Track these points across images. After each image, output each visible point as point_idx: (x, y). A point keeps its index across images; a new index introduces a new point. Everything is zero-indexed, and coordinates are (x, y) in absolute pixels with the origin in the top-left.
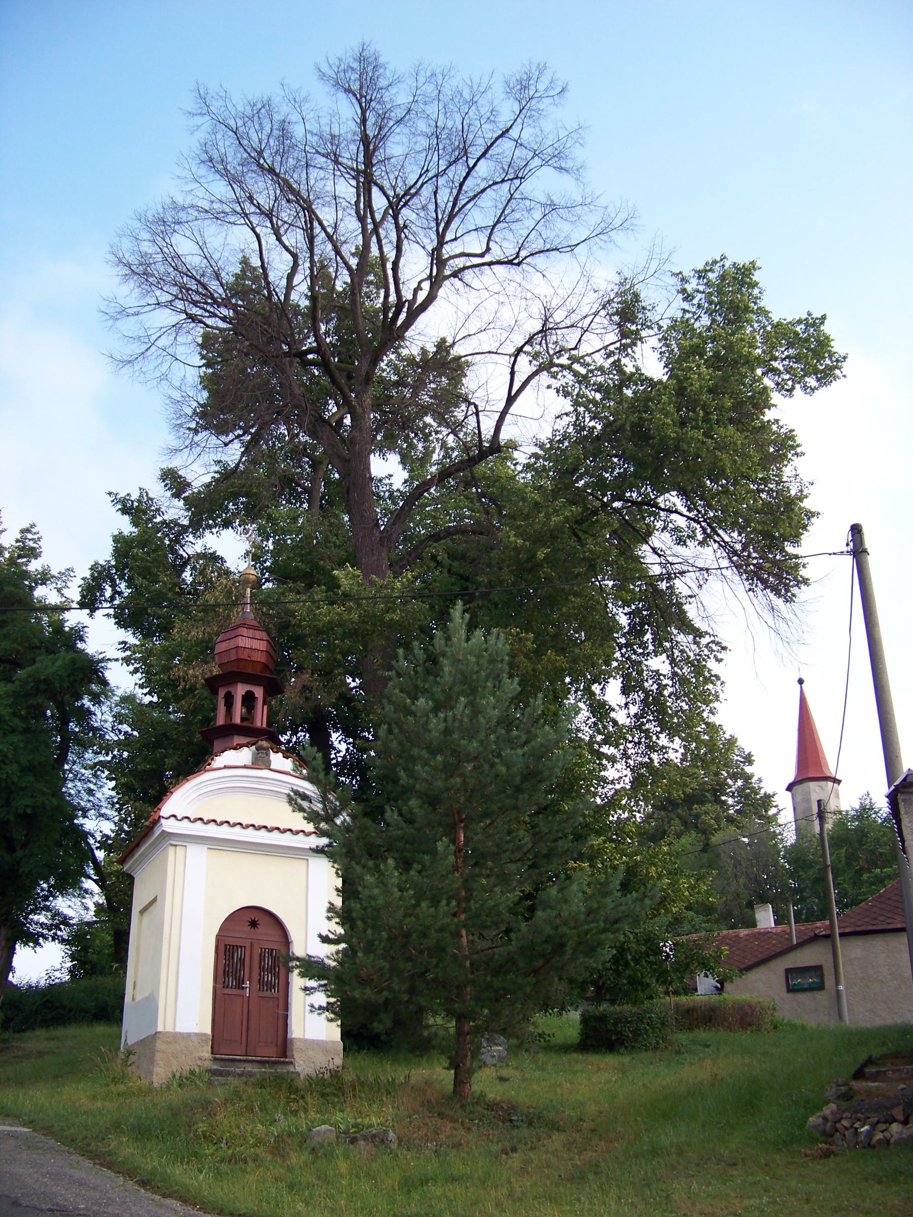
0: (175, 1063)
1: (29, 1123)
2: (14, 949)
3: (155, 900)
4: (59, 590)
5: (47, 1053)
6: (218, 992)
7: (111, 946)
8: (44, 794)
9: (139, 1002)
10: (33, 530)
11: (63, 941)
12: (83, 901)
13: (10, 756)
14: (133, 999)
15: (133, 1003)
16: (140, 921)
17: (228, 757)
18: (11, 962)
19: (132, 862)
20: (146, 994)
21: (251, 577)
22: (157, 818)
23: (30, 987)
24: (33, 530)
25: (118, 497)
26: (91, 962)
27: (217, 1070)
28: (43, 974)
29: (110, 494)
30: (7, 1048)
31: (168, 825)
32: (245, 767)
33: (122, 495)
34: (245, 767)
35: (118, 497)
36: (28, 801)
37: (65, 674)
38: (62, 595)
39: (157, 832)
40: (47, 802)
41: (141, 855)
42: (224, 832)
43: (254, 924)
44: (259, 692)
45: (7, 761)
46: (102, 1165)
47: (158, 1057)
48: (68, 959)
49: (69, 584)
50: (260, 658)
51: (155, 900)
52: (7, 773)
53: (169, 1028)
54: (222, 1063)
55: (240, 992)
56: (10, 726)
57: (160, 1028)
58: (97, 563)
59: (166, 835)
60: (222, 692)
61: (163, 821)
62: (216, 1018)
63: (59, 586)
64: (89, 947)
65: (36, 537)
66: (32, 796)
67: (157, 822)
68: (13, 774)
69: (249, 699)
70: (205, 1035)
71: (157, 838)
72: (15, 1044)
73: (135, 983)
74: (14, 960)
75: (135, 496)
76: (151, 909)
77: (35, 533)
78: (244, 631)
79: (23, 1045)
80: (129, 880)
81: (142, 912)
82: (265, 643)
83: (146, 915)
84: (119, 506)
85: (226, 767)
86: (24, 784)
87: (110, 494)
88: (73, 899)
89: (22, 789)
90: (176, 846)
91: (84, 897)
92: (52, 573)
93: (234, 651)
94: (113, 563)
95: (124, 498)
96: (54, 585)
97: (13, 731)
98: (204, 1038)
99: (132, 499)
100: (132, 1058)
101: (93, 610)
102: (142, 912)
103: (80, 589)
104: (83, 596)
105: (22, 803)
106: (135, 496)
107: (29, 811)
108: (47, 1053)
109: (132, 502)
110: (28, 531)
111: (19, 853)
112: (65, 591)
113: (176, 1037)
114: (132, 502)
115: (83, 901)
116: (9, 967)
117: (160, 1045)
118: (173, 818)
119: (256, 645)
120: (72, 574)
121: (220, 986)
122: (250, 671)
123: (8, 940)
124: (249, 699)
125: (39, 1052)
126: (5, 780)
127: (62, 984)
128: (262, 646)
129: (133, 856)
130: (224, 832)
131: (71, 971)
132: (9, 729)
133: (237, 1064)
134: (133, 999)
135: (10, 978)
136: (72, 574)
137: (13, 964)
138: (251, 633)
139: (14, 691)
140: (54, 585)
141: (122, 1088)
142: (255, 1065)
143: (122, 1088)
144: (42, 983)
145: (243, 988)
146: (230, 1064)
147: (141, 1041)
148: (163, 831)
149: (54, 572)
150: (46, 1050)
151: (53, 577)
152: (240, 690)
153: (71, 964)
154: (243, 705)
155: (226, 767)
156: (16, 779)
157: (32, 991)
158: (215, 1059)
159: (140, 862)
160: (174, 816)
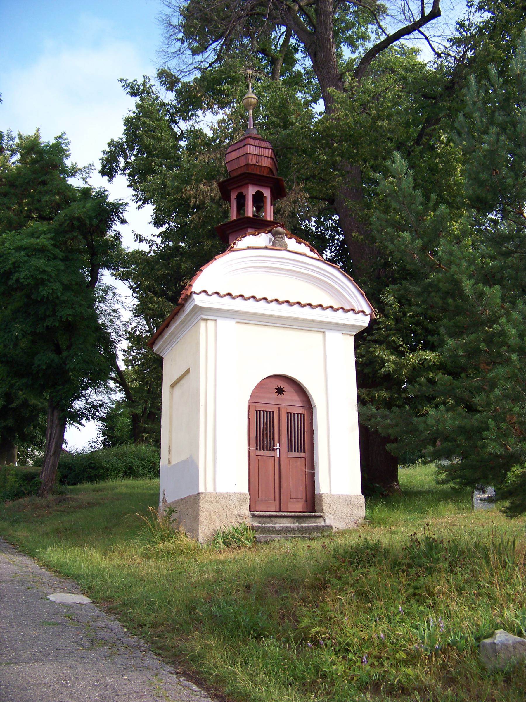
0: (218, 520)
1: (88, 590)
2: (65, 428)
3: (188, 372)
4: (84, 179)
5: (95, 504)
6: (252, 455)
7: (129, 426)
8: (81, 306)
9: (174, 465)
10: (65, 137)
11: (101, 419)
12: (110, 396)
13: (53, 275)
14: (169, 462)
15: (169, 466)
16: (171, 394)
17: (249, 240)
18: (63, 435)
19: (161, 342)
20: (183, 457)
21: (253, 100)
22: (189, 294)
23: (78, 453)
24: (65, 137)
25: (128, 82)
26: (116, 436)
27: (259, 527)
28: (87, 444)
29: (121, 80)
30: (64, 500)
31: (199, 300)
32: (266, 248)
33: (130, 81)
34: (266, 248)
35: (128, 82)
36: (70, 312)
37: (94, 215)
38: (87, 182)
39: (188, 308)
40: (84, 311)
41: (170, 335)
42: (251, 306)
43: (280, 391)
44: (267, 193)
45: (52, 280)
46: (185, 674)
47: (202, 516)
48: (101, 435)
49: (91, 175)
50: (266, 163)
51: (188, 372)
52: (52, 289)
53: (210, 489)
54: (260, 519)
55: (272, 453)
56: (52, 254)
57: (200, 491)
58: (113, 141)
59: (198, 309)
60: (234, 196)
61: (194, 296)
62: (251, 480)
63: (84, 176)
64: (114, 427)
65: (66, 141)
66: (72, 308)
67: (189, 297)
68: (57, 289)
69: (259, 199)
70: (243, 494)
71: (188, 315)
72: (69, 496)
73: (169, 448)
74: (65, 433)
75: (140, 81)
76: (183, 382)
77: (65, 139)
78: (251, 141)
79: (76, 497)
80: (159, 362)
81: (173, 386)
82: (270, 151)
83: (177, 389)
84: (129, 90)
85: (248, 248)
86: (66, 298)
87: (121, 80)
88: (103, 395)
89: (64, 302)
90: (206, 320)
91: (110, 394)
92: (79, 167)
93: (243, 158)
94: (125, 140)
95: (132, 83)
96: (81, 176)
97: (55, 258)
98: (242, 497)
99: (138, 83)
100: (174, 516)
101: (111, 177)
102: (173, 386)
103: (101, 161)
104: (104, 167)
105: (65, 313)
106: (140, 81)
107: (70, 319)
108: (95, 504)
109: (139, 86)
110: (60, 137)
111: (65, 354)
112: (88, 180)
113: (218, 497)
114: (139, 86)
115: (110, 396)
116: (61, 440)
117: (203, 505)
118: (203, 294)
119: (262, 152)
120: (93, 168)
121: (253, 448)
122: (259, 173)
123: (60, 419)
124: (259, 199)
125: (88, 503)
126: (51, 294)
127: (99, 451)
128: (269, 153)
129: (163, 337)
130: (251, 306)
131: (104, 443)
132: (52, 256)
133: (273, 519)
134: (169, 462)
135: (64, 446)
136: (93, 168)
137: (65, 438)
138: (257, 143)
139: (54, 229)
140: (81, 176)
141: (170, 545)
142: (290, 520)
143: (170, 545)
144: (87, 450)
145: (274, 450)
146: (268, 520)
147: (181, 500)
148: (196, 306)
149: (80, 166)
150: (94, 501)
151: (80, 170)
152: (251, 191)
153: (103, 438)
154: (253, 206)
155: (248, 248)
156: (59, 294)
157: (79, 457)
158: (254, 516)
159: (168, 343)
160: (205, 292)
